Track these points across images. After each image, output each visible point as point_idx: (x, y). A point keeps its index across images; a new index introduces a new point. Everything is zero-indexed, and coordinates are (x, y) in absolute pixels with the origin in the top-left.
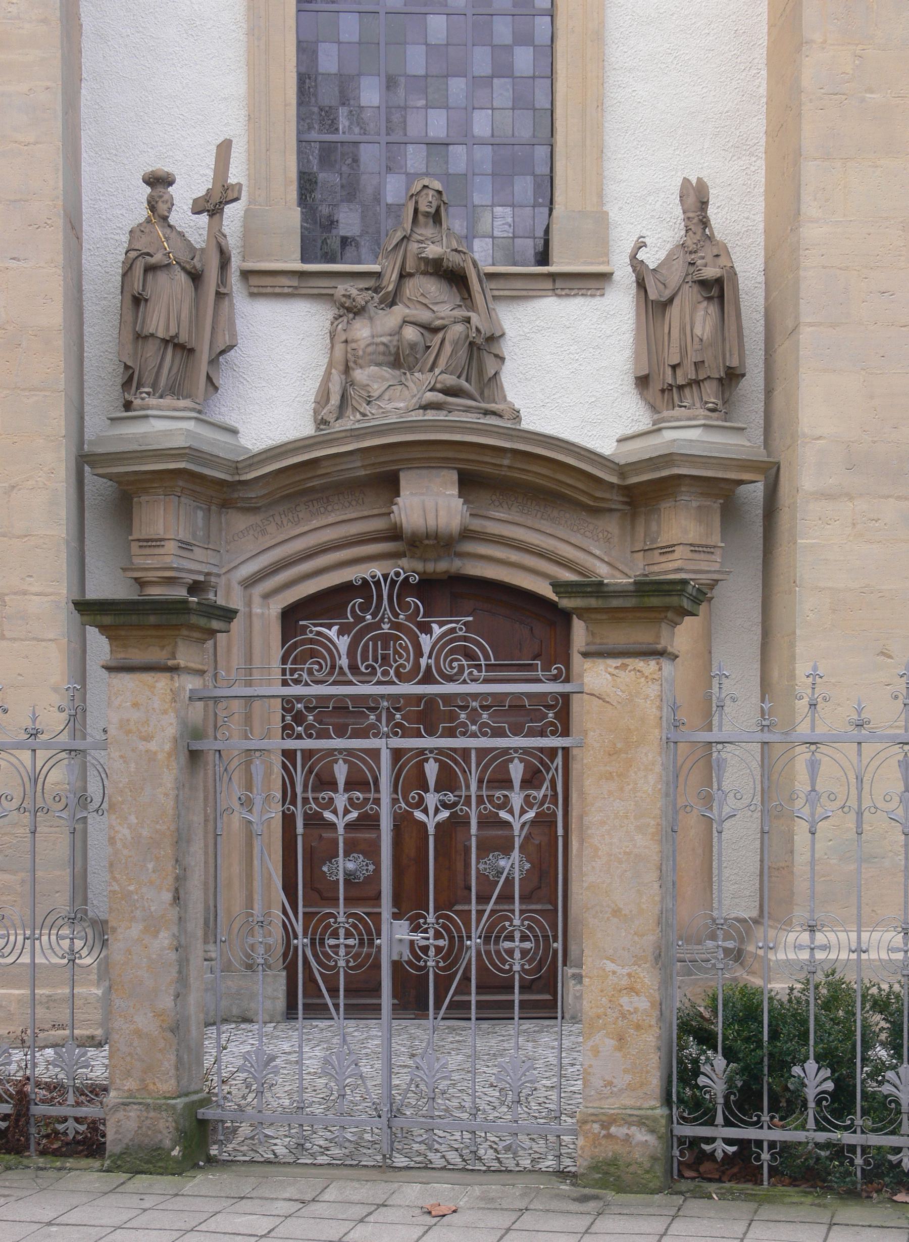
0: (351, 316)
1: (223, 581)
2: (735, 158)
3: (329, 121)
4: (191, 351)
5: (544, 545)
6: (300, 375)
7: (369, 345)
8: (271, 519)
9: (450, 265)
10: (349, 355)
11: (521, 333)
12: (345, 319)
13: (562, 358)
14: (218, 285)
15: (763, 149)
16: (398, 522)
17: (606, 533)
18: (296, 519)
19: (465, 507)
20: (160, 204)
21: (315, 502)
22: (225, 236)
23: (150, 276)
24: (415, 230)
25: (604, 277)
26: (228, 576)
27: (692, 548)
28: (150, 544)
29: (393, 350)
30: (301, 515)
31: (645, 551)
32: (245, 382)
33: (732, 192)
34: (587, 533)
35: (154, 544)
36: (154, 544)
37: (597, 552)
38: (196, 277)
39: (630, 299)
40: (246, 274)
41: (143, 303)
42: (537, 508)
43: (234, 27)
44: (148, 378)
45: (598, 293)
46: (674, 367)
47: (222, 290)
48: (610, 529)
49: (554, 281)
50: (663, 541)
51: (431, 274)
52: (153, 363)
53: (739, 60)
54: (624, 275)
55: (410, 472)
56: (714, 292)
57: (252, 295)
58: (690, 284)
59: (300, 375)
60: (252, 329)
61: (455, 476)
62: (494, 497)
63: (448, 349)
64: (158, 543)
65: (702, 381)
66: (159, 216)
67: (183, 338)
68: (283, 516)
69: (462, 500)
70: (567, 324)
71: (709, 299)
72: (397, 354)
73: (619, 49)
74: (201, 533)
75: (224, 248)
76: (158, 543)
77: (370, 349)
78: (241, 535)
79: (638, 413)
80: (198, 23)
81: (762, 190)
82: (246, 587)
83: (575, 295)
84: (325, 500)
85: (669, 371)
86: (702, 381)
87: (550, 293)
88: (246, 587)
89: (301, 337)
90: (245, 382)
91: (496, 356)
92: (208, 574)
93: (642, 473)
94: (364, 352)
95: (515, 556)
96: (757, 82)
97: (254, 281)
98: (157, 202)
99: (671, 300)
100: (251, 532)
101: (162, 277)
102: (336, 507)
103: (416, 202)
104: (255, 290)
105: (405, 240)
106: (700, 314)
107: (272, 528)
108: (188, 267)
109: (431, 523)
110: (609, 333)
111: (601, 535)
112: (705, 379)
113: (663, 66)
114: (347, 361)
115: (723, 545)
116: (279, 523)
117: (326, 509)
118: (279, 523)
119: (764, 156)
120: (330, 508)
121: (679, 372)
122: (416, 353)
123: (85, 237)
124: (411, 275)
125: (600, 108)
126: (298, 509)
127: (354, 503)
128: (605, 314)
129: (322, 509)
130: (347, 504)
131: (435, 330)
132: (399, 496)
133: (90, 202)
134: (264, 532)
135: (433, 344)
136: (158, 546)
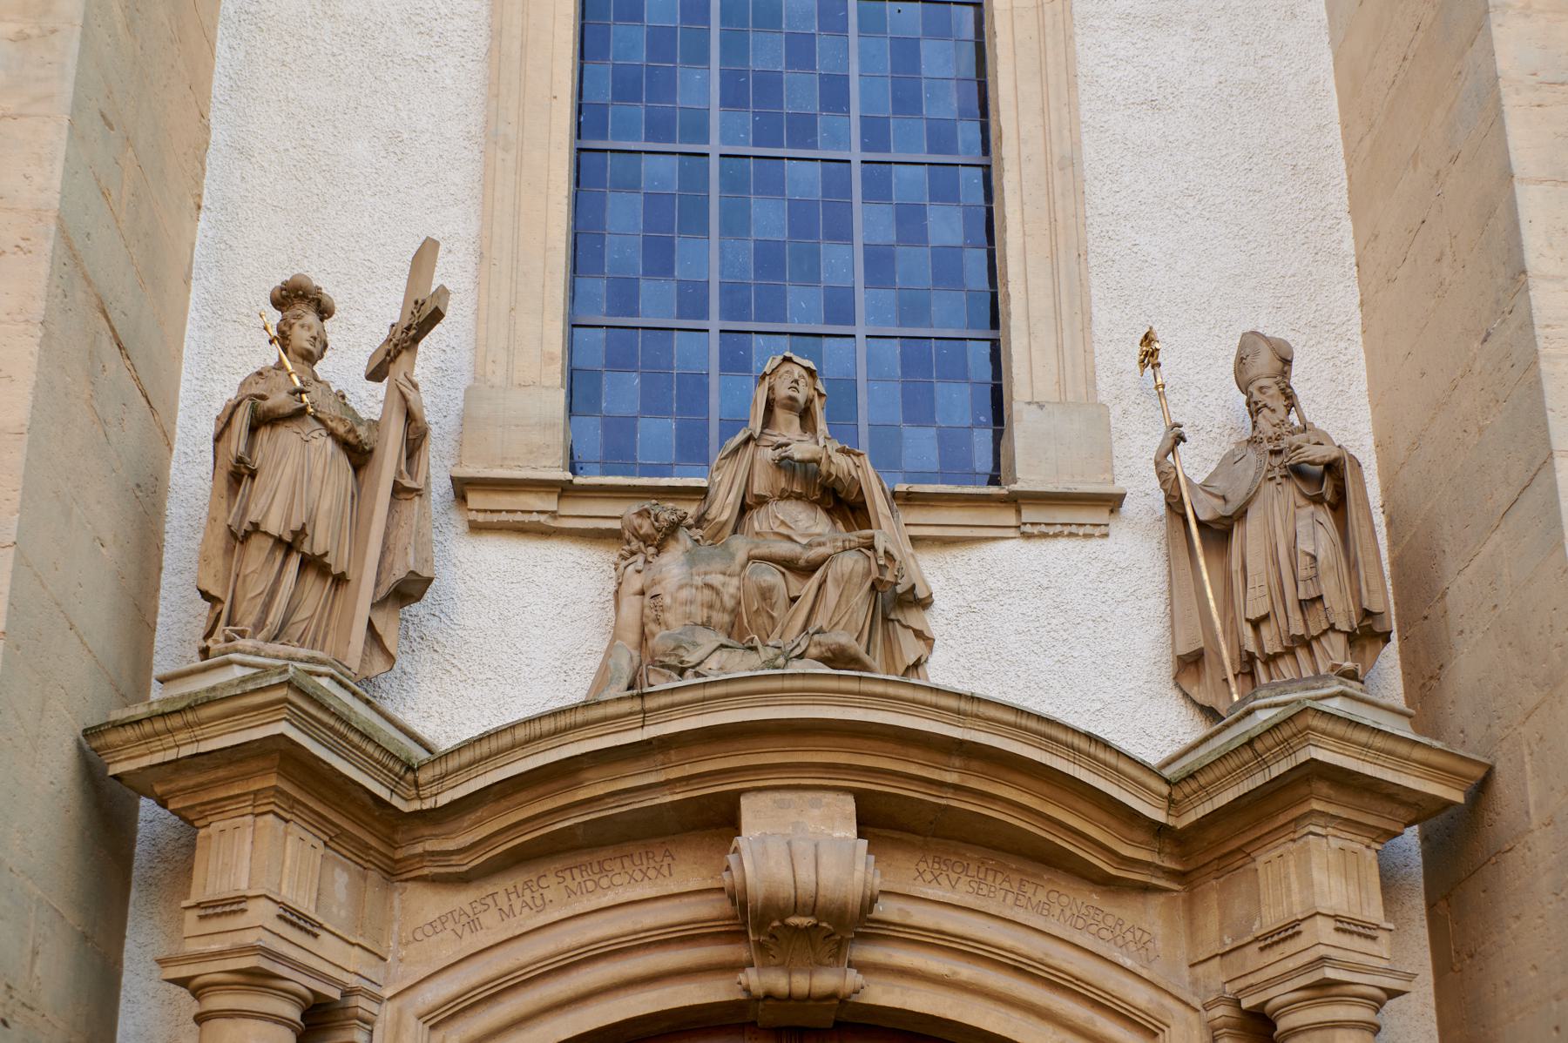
0: (652, 550)
1: (386, 1013)
2: (1311, 343)
3: (624, 296)
4: (340, 580)
5: (1024, 949)
6: (558, 663)
7: (681, 587)
8: (489, 901)
9: (833, 470)
10: (647, 611)
11: (961, 602)
12: (640, 558)
13: (1036, 638)
14: (400, 473)
15: (1358, 329)
16: (738, 887)
17: (1139, 933)
18: (539, 902)
19: (872, 858)
20: (296, 328)
21: (575, 871)
22: (415, 386)
23: (264, 434)
24: (767, 431)
25: (1112, 502)
26: (397, 1003)
27: (1339, 925)
28: (219, 910)
29: (730, 603)
30: (548, 895)
31: (1222, 955)
32: (454, 671)
33: (1313, 391)
34: (1104, 933)
35: (227, 909)
36: (227, 909)
37: (1128, 963)
38: (358, 455)
39: (1155, 544)
40: (462, 488)
41: (246, 481)
42: (1006, 885)
43: (466, 143)
44: (248, 617)
45: (1097, 531)
46: (1256, 624)
47: (407, 482)
48: (1145, 926)
49: (1019, 512)
50: (1271, 918)
51: (799, 497)
52: (257, 586)
53: (1303, 206)
54: (1144, 497)
55: (765, 799)
56: (1327, 488)
57: (476, 528)
58: (1279, 479)
59: (558, 663)
60: (470, 583)
61: (849, 805)
62: (922, 866)
63: (832, 592)
64: (234, 907)
65: (1317, 638)
66: (294, 351)
67: (320, 542)
68: (513, 897)
69: (864, 843)
70: (1045, 583)
71: (1317, 500)
72: (735, 613)
73: (1106, 188)
74: (343, 913)
75: (415, 408)
76: (234, 907)
77: (685, 594)
78: (429, 930)
79: (1181, 730)
80: (405, 136)
81: (1364, 387)
82: (432, 1027)
83: (1056, 536)
84: (596, 868)
85: (1248, 631)
86: (1317, 638)
87: (1011, 533)
88: (432, 1027)
89: (562, 601)
90: (454, 671)
91: (919, 634)
92: (348, 993)
93: (1219, 791)
94: (674, 599)
95: (966, 971)
96: (1336, 236)
97: (476, 499)
98: (291, 327)
99: (1241, 514)
100: (450, 925)
101: (287, 436)
102: (617, 880)
103: (771, 389)
104: (481, 518)
105: (752, 445)
106: (1303, 526)
107: (490, 918)
108: (341, 430)
109: (806, 876)
110: (1119, 596)
111: (1129, 936)
112: (1325, 632)
113: (1180, 212)
114: (643, 625)
115: (1391, 926)
116: (506, 908)
117: (597, 884)
118: (506, 908)
119: (1360, 340)
120: (604, 882)
121: (1265, 631)
122: (772, 607)
123: (179, 433)
124: (762, 501)
125: (1082, 257)
126: (543, 883)
127: (652, 873)
128: (1111, 567)
129: (590, 885)
130: (638, 876)
131: (808, 570)
132: (739, 834)
133: (195, 382)
134: (474, 924)
135: (803, 592)
136: (234, 912)
